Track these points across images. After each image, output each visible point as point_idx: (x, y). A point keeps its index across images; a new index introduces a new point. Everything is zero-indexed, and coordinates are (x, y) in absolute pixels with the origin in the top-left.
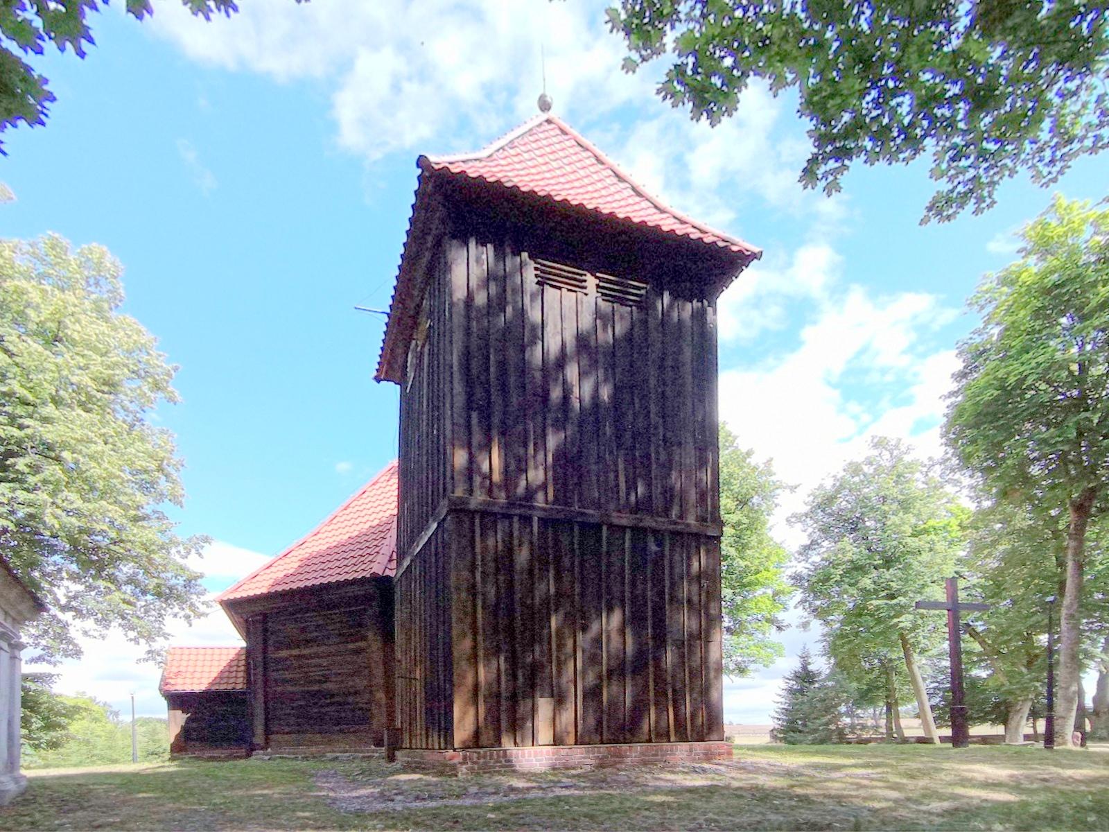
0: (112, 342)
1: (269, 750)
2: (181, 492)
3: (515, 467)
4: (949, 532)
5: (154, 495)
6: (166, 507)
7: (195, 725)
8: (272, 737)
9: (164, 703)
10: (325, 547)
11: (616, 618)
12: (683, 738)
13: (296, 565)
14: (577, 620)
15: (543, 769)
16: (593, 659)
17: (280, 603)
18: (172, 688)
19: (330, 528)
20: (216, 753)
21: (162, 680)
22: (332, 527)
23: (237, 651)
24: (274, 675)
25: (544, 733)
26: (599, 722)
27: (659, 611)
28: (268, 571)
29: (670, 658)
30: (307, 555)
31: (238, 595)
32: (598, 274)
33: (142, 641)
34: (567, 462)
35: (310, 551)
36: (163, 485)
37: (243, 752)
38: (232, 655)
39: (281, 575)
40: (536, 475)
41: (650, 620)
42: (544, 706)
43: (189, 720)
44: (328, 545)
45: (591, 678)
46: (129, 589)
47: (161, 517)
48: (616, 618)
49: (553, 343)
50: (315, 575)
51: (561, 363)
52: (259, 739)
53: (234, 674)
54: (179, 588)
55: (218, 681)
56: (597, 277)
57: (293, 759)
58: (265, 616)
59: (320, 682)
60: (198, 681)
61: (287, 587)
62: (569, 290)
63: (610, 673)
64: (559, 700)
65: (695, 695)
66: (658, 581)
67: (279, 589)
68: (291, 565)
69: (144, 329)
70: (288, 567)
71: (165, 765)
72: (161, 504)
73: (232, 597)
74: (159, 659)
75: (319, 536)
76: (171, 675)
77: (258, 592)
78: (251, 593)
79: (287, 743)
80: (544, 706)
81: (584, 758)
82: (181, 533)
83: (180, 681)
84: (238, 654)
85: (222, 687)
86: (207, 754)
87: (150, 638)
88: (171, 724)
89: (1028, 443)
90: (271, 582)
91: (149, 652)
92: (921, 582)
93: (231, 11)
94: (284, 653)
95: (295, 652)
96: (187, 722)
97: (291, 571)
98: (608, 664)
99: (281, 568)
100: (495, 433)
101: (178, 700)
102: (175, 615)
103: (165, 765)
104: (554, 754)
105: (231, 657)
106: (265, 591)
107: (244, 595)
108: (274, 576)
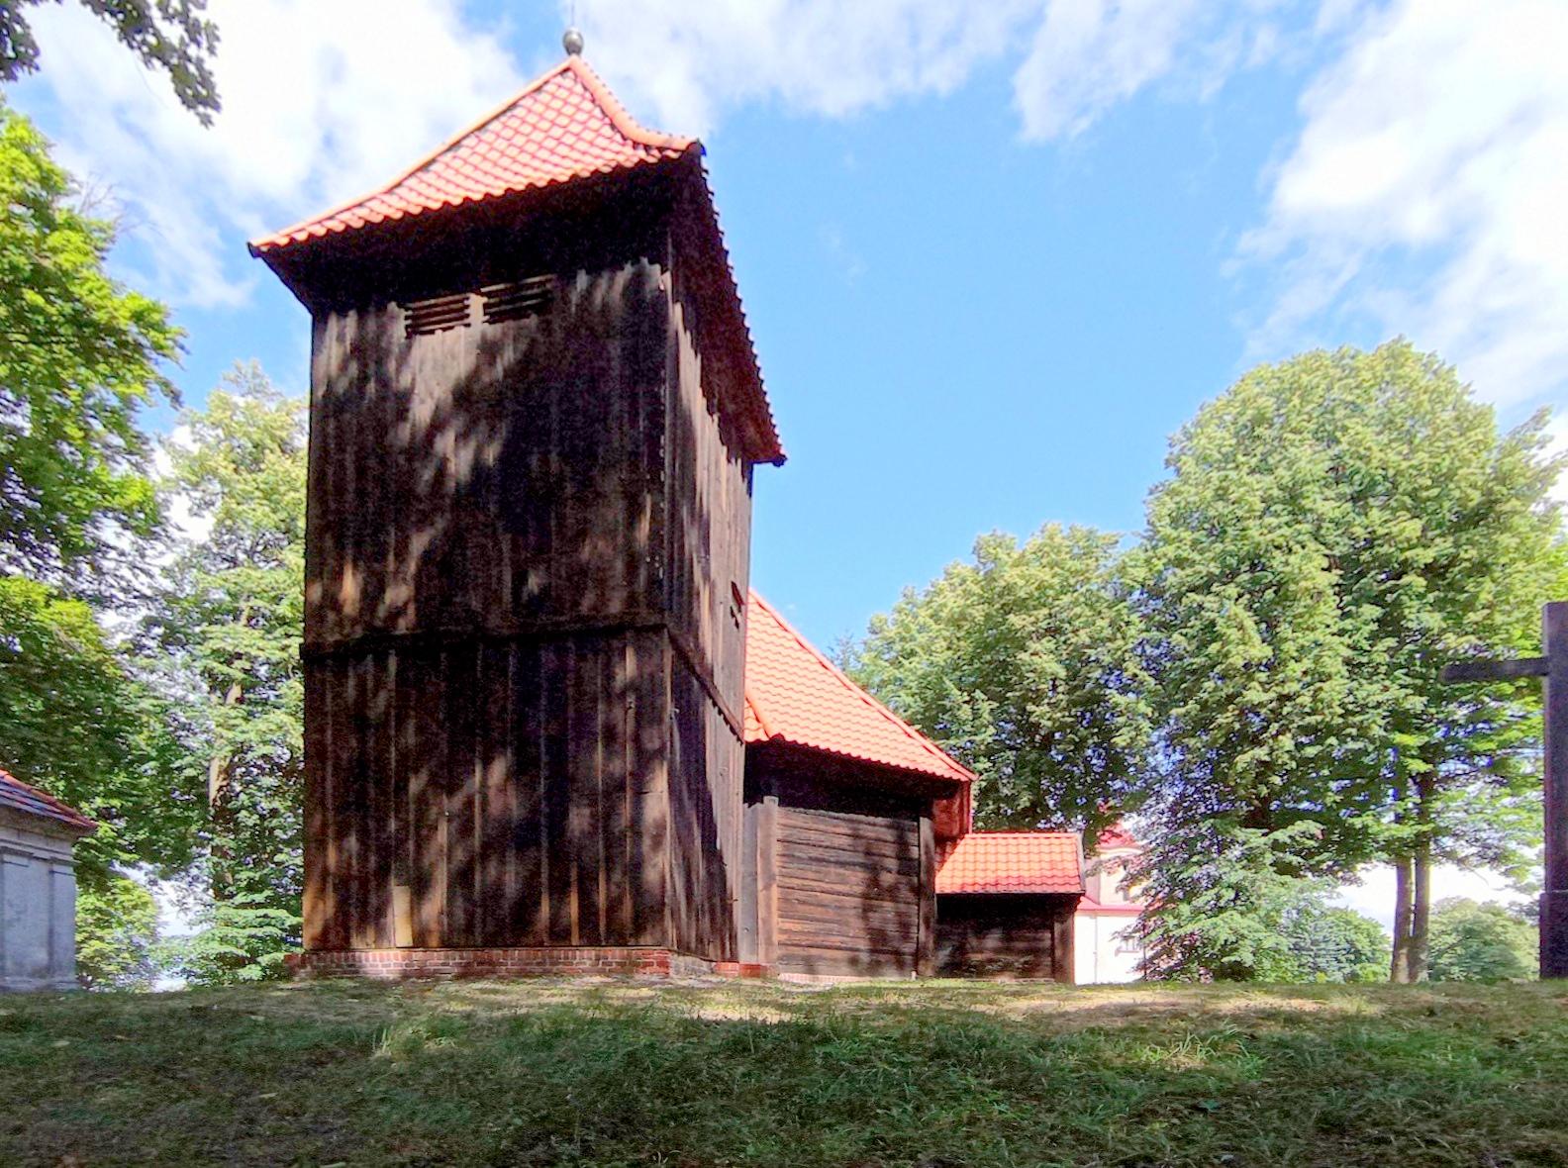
3: (372, 595)
4: (1143, 616)
11: (499, 769)
12: (592, 939)
14: (448, 780)
15: (391, 977)
16: (466, 830)
25: (400, 930)
26: (470, 916)
27: (557, 746)
29: (579, 819)
32: (483, 290)
34: (440, 568)
40: (398, 594)
41: (550, 773)
42: (399, 899)
45: (460, 855)
48: (499, 769)
49: (422, 412)
51: (437, 426)
56: (483, 295)
62: (444, 330)
63: (486, 846)
64: (420, 887)
65: (617, 877)
66: (557, 710)
80: (399, 899)
81: (443, 964)
92: (1060, 689)
93: (33, 70)
98: (484, 834)
100: (349, 543)
104: (404, 959)
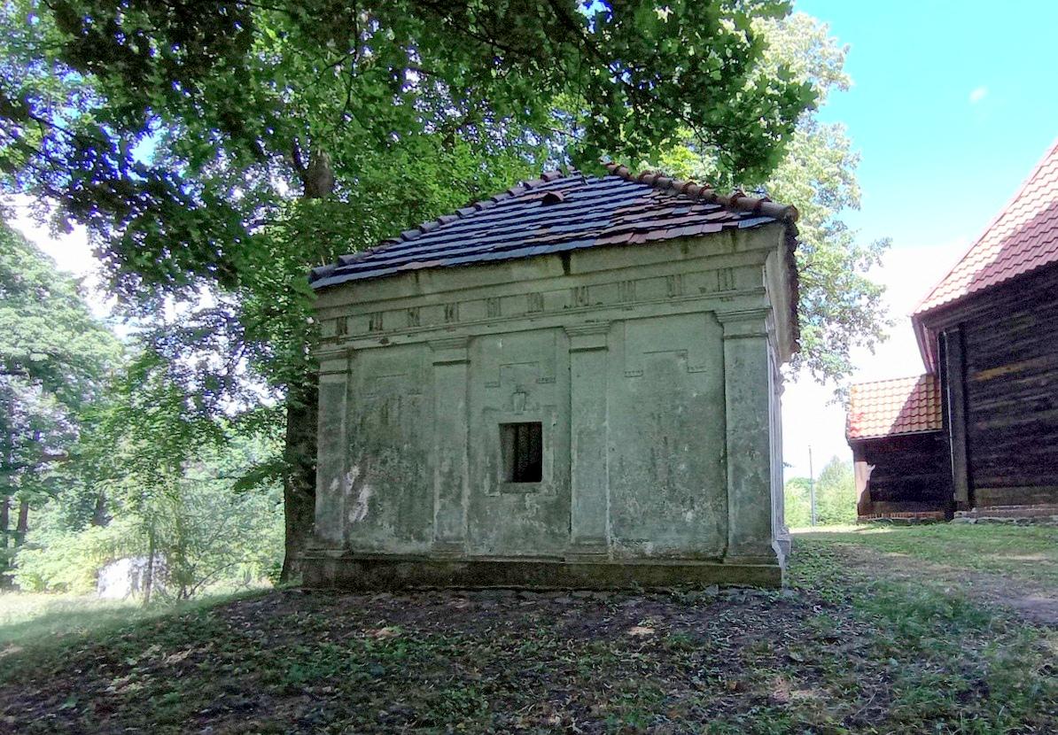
0: (794, 47)
1: (974, 510)
2: (859, 191)
5: (835, 203)
6: (846, 215)
7: (880, 480)
8: (978, 492)
9: (848, 454)
10: (1033, 215)
13: (998, 249)
17: (972, 309)
18: (857, 435)
19: (1034, 187)
20: (902, 516)
21: (847, 425)
22: (1039, 183)
23: (916, 381)
24: (975, 406)
28: (963, 265)
30: (1010, 233)
31: (933, 304)
33: (830, 379)
35: (1012, 225)
36: (842, 190)
37: (942, 514)
38: (910, 386)
39: (981, 266)
43: (874, 474)
44: (1037, 211)
46: (210, 577)
47: (840, 227)
50: (1027, 256)
52: (961, 495)
53: (916, 412)
54: (863, 309)
55: (900, 421)
57: (1006, 523)
58: (961, 325)
59: (1037, 409)
60: (879, 425)
61: (991, 281)
67: (982, 285)
68: (991, 252)
69: (813, 19)
70: (987, 254)
71: (847, 525)
72: (841, 211)
73: (926, 307)
74: (845, 399)
75: (1022, 201)
76: (855, 419)
77: (956, 295)
78: (948, 298)
79: (998, 502)
82: (862, 243)
83: (863, 425)
84: (918, 385)
85: (906, 429)
86: (894, 516)
87: (837, 377)
88: (855, 478)
89: (510, 436)
90: (970, 279)
91: (837, 392)
94: (988, 374)
95: (1001, 371)
96: (871, 476)
97: (994, 258)
99: (979, 258)
101: (865, 449)
102: (859, 344)
103: (847, 525)
105: (911, 389)
106: (963, 292)
107: (940, 302)
108: (972, 270)
